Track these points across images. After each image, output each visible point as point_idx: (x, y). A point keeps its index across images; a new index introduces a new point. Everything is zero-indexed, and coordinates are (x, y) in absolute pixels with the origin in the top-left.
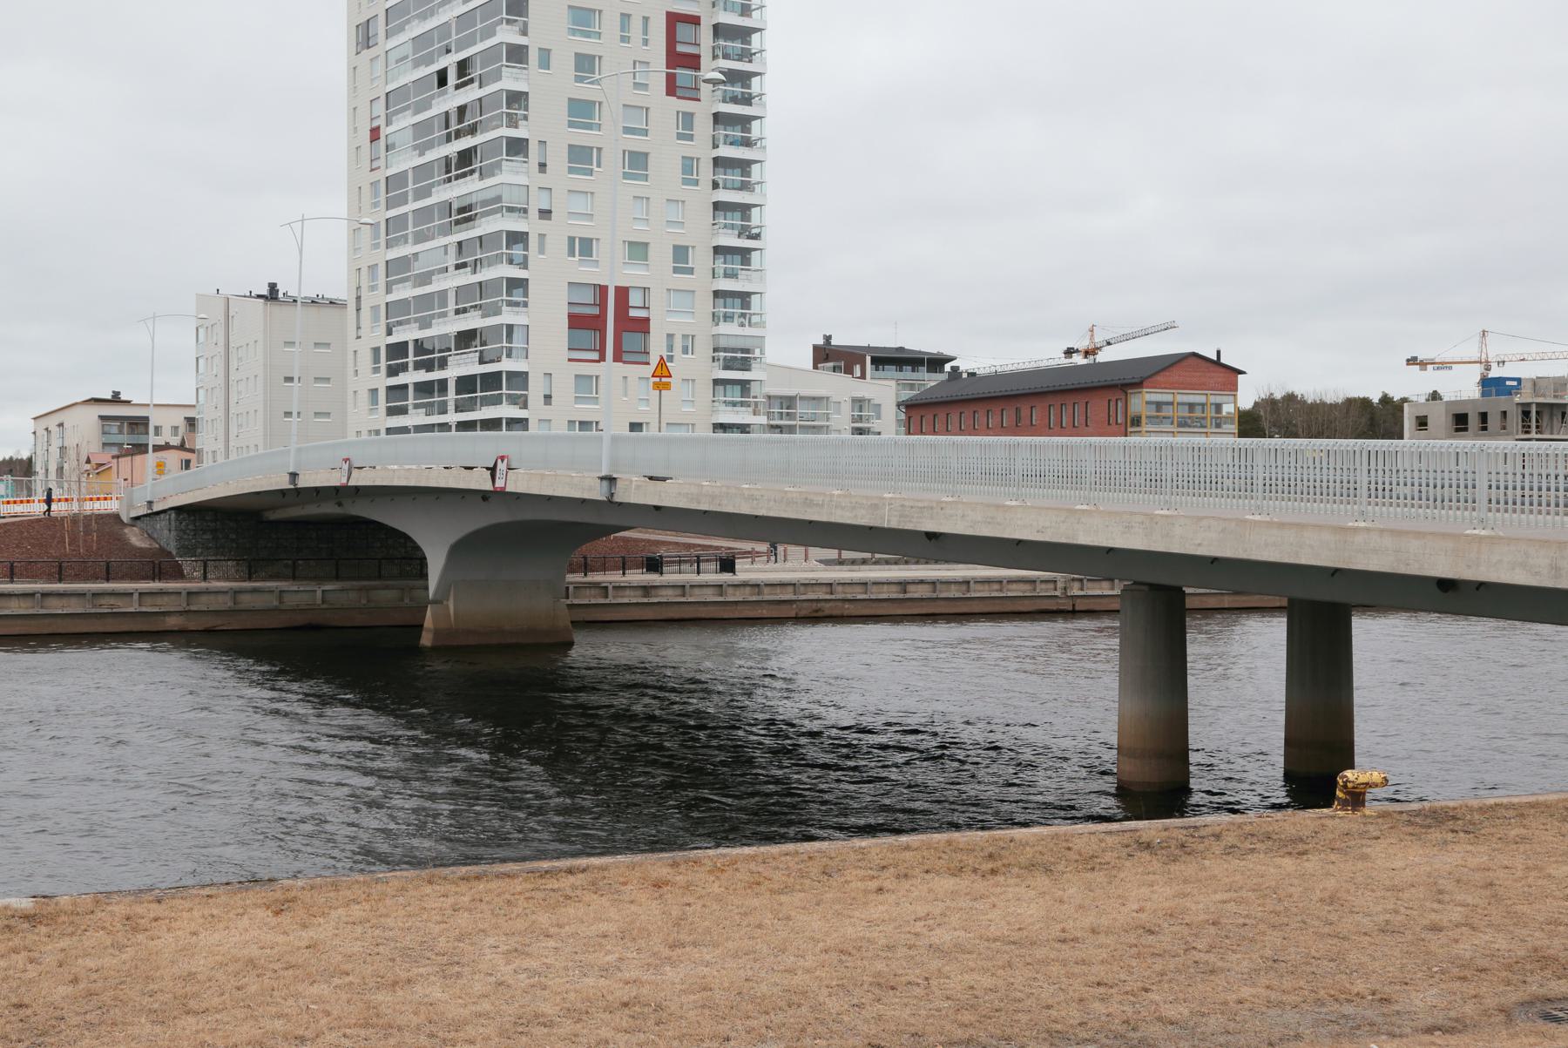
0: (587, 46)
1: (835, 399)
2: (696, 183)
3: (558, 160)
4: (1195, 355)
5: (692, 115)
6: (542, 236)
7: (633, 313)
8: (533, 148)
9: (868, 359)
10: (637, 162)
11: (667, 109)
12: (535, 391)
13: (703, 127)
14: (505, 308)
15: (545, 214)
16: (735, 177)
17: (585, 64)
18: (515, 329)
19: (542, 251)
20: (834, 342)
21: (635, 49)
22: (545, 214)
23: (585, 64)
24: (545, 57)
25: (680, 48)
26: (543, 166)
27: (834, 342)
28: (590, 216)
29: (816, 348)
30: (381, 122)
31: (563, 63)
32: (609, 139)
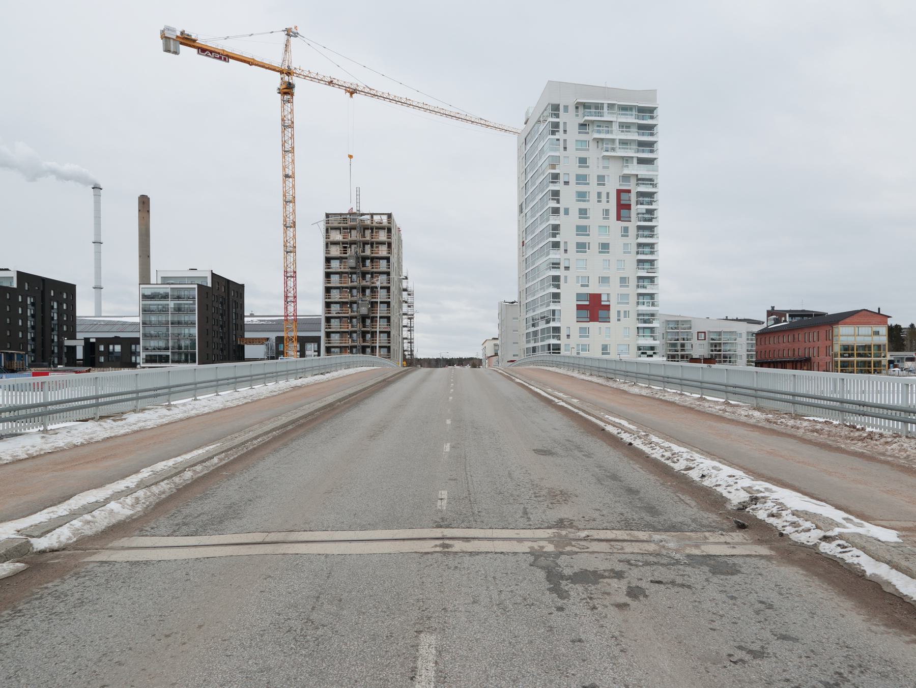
0: (583, 205)
1: (739, 332)
2: (630, 253)
3: (572, 248)
4: (864, 310)
5: (628, 227)
6: (566, 277)
7: (603, 303)
8: (562, 245)
9: (787, 315)
10: (605, 247)
11: (616, 226)
12: (563, 334)
13: (633, 231)
14: (551, 304)
15: (567, 268)
16: (647, 250)
17: (583, 213)
18: (556, 312)
19: (566, 282)
20: (775, 309)
21: (604, 205)
22: (567, 268)
23: (583, 213)
24: (567, 212)
25: (622, 202)
26: (566, 251)
27: (775, 309)
28: (586, 268)
29: (768, 312)
30: (524, 239)
31: (574, 212)
32: (594, 239)
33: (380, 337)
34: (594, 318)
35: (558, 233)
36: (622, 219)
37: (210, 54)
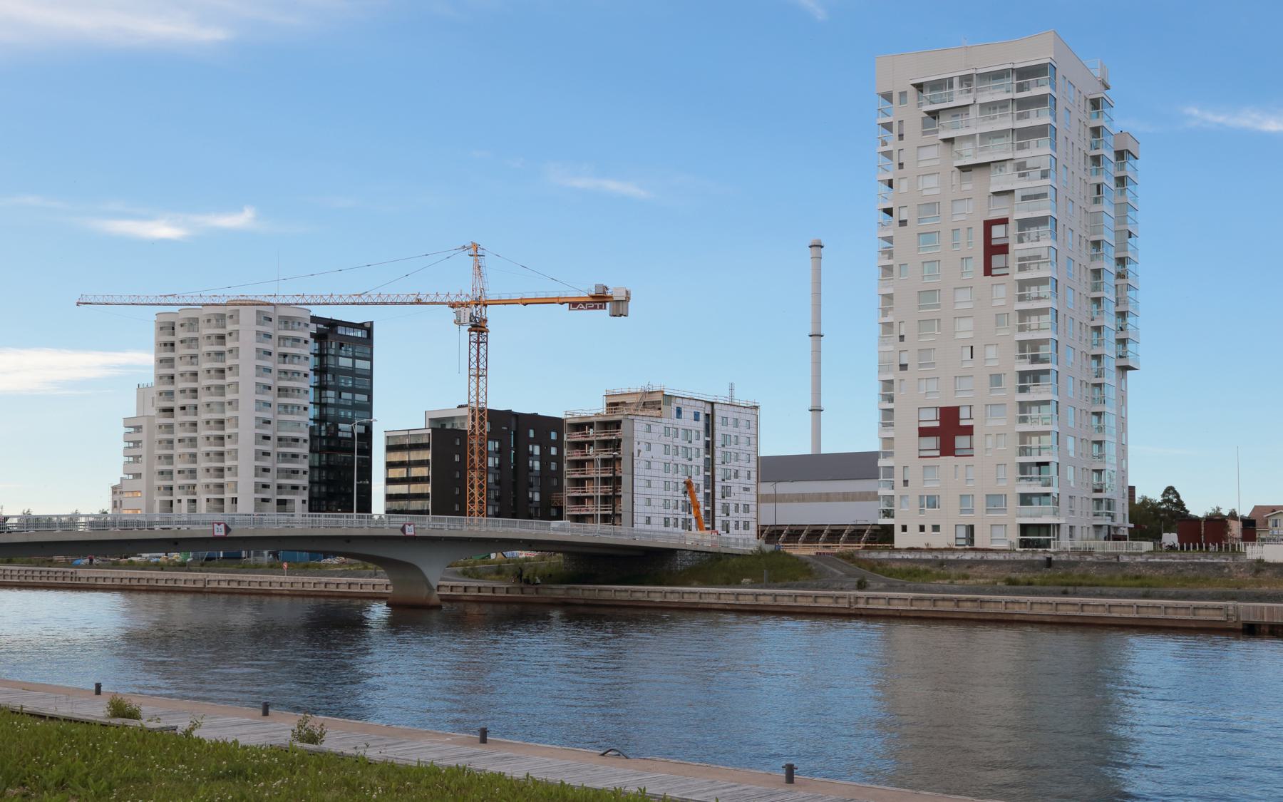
7: (962, 423)
25: (994, 243)
33: (428, 506)
34: (947, 449)
35: (891, 309)
36: (994, 272)
37: (583, 307)
